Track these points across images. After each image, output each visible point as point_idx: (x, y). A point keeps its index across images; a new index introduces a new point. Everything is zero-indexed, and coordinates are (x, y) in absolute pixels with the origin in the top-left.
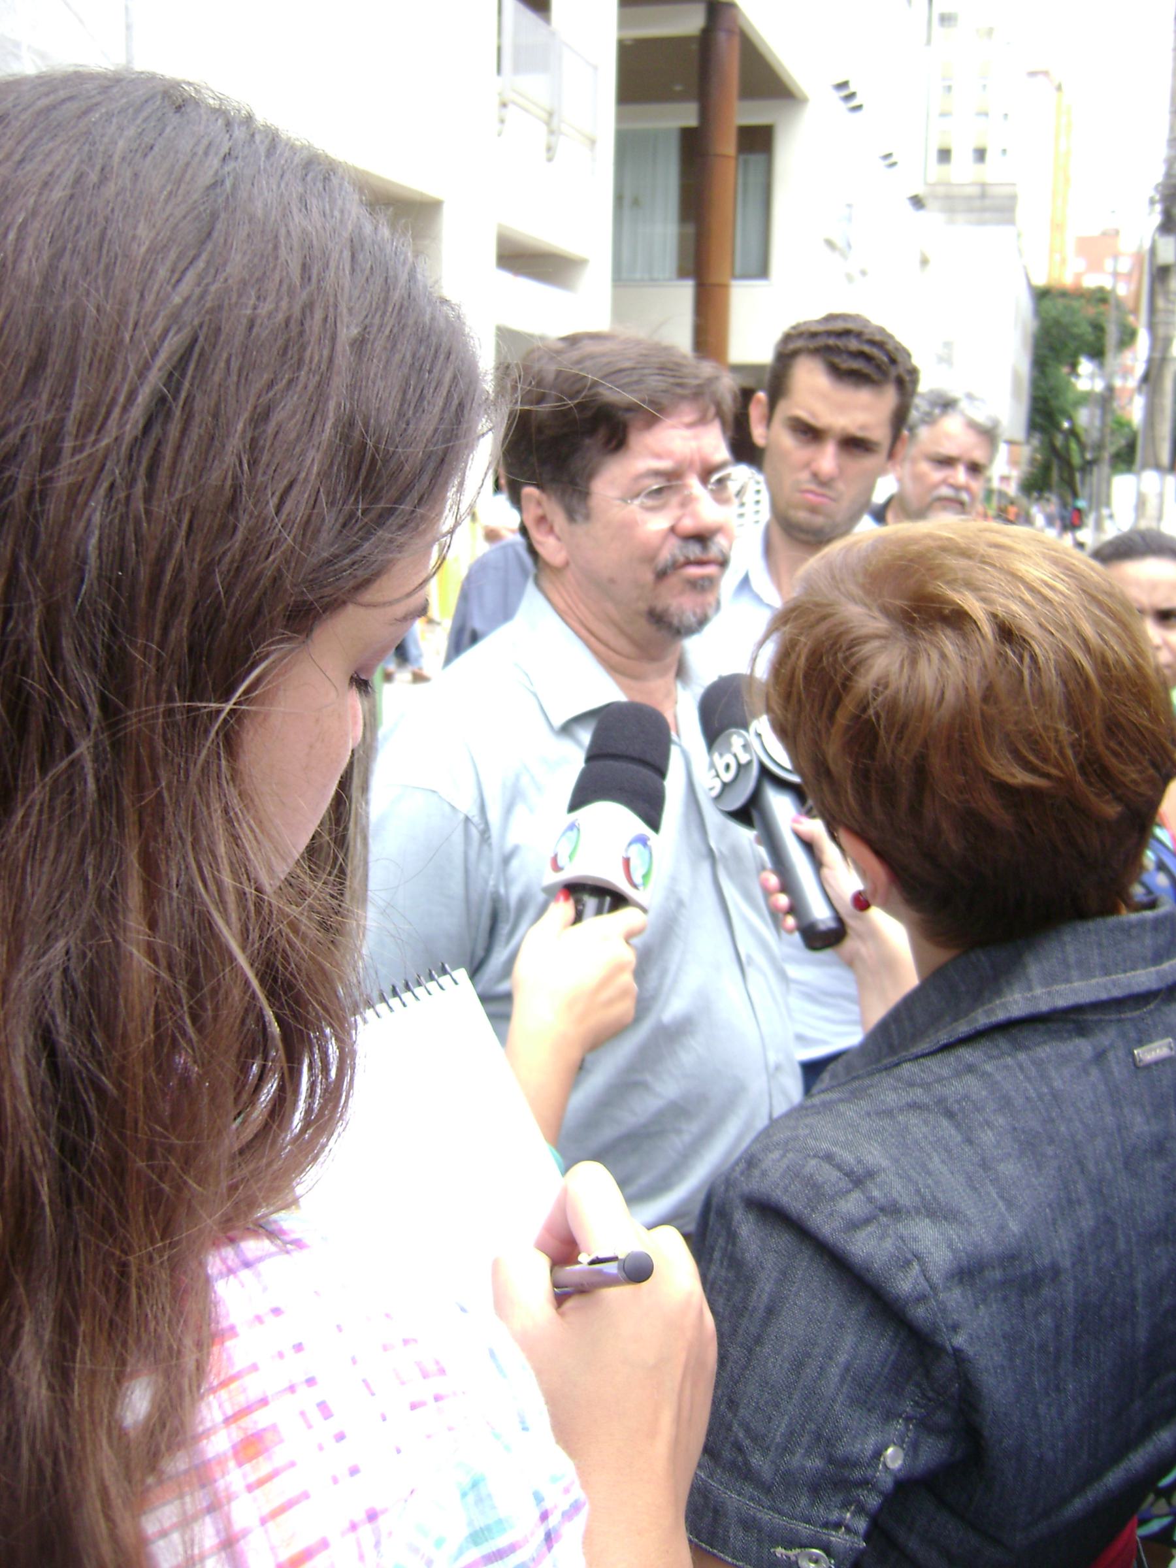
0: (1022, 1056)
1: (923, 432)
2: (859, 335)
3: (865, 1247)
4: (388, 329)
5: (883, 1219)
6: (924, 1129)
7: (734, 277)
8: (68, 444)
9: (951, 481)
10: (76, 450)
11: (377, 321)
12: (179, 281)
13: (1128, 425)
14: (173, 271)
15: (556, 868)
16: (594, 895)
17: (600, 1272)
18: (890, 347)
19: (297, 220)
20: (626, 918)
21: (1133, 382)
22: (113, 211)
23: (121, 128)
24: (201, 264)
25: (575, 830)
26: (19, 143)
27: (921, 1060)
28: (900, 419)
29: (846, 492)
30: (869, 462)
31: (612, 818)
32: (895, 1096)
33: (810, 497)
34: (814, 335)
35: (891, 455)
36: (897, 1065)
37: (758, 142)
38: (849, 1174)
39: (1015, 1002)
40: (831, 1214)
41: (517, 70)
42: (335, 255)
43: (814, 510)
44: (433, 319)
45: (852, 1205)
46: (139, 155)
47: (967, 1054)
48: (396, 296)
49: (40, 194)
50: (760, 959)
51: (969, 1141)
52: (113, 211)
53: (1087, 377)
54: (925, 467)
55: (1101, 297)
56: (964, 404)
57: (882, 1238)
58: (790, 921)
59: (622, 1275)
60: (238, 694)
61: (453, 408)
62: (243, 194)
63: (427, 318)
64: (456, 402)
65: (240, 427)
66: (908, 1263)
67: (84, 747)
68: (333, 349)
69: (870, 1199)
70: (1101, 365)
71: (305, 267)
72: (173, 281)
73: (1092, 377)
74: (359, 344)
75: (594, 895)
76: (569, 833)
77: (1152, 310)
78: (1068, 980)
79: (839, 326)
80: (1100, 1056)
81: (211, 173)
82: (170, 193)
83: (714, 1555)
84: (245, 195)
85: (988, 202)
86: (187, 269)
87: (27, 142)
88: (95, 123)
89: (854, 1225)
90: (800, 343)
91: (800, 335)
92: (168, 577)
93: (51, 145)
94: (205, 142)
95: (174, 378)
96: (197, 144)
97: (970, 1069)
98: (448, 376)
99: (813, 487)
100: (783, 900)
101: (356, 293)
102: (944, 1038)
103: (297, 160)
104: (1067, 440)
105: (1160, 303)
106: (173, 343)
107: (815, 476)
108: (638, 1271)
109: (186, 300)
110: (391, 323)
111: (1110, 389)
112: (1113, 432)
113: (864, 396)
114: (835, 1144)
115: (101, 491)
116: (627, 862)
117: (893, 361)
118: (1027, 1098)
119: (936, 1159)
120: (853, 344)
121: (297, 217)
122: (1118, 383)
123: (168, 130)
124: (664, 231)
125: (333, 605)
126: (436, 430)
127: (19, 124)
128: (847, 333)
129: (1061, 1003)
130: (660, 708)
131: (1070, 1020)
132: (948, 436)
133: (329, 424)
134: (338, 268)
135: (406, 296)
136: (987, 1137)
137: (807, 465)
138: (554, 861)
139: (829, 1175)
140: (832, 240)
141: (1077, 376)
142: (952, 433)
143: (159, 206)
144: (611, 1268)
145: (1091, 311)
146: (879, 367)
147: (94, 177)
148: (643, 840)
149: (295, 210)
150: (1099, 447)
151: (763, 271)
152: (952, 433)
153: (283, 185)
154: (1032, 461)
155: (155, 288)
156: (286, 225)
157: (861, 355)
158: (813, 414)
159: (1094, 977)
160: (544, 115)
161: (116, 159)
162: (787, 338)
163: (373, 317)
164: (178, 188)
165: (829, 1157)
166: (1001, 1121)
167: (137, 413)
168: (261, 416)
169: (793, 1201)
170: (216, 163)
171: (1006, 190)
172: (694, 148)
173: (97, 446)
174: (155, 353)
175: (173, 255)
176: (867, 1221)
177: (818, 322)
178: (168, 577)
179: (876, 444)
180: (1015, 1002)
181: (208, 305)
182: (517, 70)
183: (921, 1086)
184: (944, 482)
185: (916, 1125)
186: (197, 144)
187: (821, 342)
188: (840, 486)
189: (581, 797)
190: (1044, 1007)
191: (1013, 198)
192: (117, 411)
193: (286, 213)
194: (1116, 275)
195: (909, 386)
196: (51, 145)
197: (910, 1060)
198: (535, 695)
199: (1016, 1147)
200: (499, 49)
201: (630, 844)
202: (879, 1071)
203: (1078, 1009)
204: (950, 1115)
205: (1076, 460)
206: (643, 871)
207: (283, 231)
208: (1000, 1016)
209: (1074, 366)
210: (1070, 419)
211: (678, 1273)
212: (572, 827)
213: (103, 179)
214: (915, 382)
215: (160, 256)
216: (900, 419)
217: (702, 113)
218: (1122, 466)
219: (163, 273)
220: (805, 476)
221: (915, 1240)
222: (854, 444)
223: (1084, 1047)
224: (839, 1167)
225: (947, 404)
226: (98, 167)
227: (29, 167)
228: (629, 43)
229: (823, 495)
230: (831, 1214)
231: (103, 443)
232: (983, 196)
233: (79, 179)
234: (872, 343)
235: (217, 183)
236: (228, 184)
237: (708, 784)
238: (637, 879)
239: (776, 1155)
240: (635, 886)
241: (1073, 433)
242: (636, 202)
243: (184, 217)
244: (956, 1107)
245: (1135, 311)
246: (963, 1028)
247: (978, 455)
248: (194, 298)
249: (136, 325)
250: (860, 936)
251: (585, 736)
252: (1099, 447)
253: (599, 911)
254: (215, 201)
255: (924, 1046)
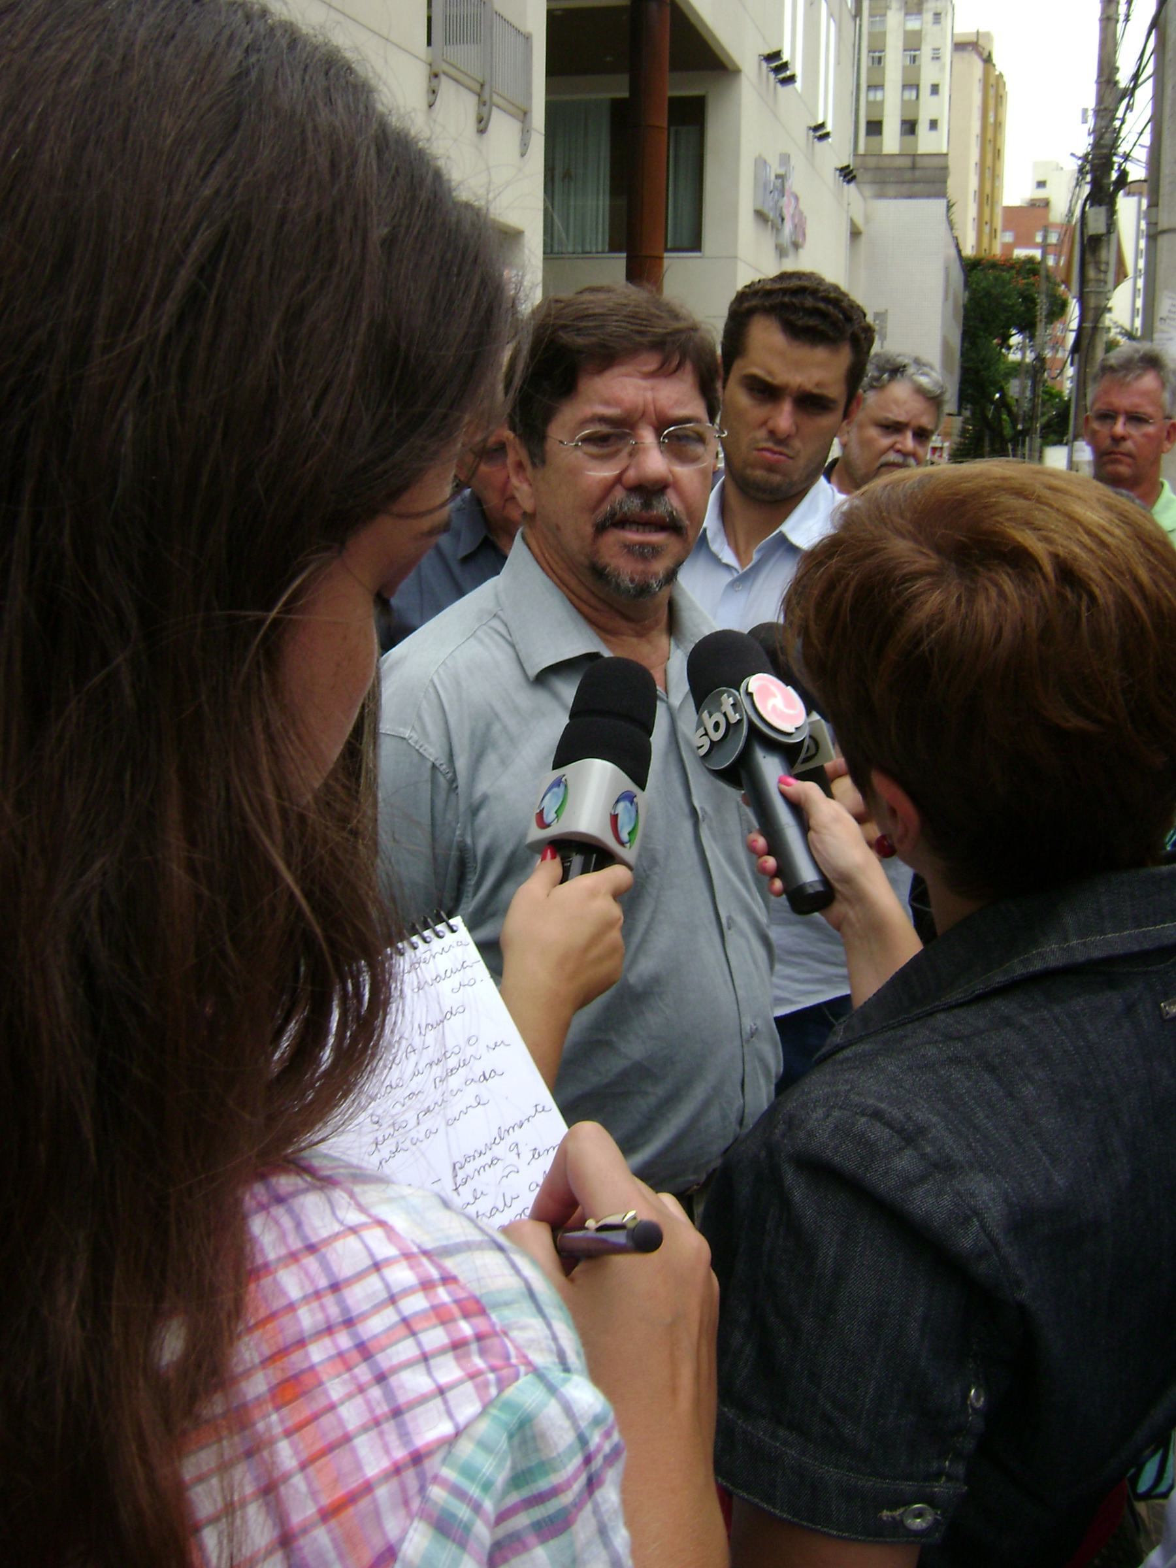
0: (1057, 1010)
1: (871, 398)
2: (814, 292)
3: (928, 1203)
4: (416, 231)
5: (938, 1176)
6: (967, 1084)
7: (667, 250)
8: (99, 341)
9: (899, 446)
10: (107, 349)
11: (404, 221)
12: (207, 174)
13: (1059, 395)
14: (200, 164)
15: (543, 824)
16: (581, 853)
17: (604, 1241)
18: (845, 304)
19: (323, 114)
20: (616, 874)
21: (1063, 354)
22: (136, 100)
23: (141, 16)
24: (230, 155)
25: (562, 787)
26: (33, 31)
27: (956, 1011)
28: (854, 376)
29: (803, 449)
30: (827, 421)
31: (598, 776)
32: (935, 1050)
33: (768, 455)
34: (769, 293)
35: (846, 415)
36: (931, 1014)
37: (691, 115)
38: (900, 1131)
39: (1051, 953)
40: (887, 1173)
41: (447, 41)
42: (363, 153)
43: (771, 468)
44: (458, 222)
45: (905, 1162)
46: (160, 44)
47: (1003, 1006)
48: (423, 195)
49: (59, 82)
50: (742, 922)
51: (1010, 1095)
52: (136, 100)
53: (1017, 350)
54: (873, 432)
55: (1030, 268)
56: (911, 370)
57: (939, 1194)
58: (778, 884)
59: (630, 1244)
60: (280, 604)
61: (482, 313)
62: (268, 87)
63: (454, 219)
64: (484, 306)
65: (274, 326)
66: (967, 1219)
67: (120, 659)
68: (364, 247)
69: (923, 1156)
70: (1032, 337)
71: (333, 165)
72: (201, 174)
73: (1022, 349)
74: (389, 243)
75: (581, 853)
76: (555, 790)
77: (1083, 281)
78: (1103, 932)
79: (794, 283)
80: (1130, 1009)
81: (235, 65)
82: (195, 82)
83: (817, 1531)
84: (270, 87)
85: (918, 174)
86: (214, 162)
87: (43, 30)
88: (112, 11)
89: (910, 1183)
90: (754, 302)
91: (755, 293)
92: (204, 480)
93: (68, 33)
94: (227, 33)
95: (205, 271)
96: (219, 34)
97: (1007, 1021)
98: (477, 281)
99: (770, 445)
100: (771, 862)
101: (384, 192)
102: (979, 988)
103: (318, 55)
104: (998, 410)
105: (1091, 273)
106: (205, 235)
107: (772, 433)
108: (647, 1239)
109: (217, 192)
110: (419, 223)
111: (1040, 359)
112: (1044, 403)
113: (820, 354)
114: (880, 1099)
115: (133, 392)
116: (614, 818)
117: (848, 319)
118: (1065, 1051)
119: (981, 1115)
120: (809, 302)
121: (324, 112)
122: (1048, 354)
123: (189, 18)
124: (596, 204)
125: (371, 512)
126: (466, 335)
127: (31, 11)
128: (802, 290)
129: (1096, 954)
130: (645, 663)
131: (1100, 973)
132: (896, 402)
133: (363, 326)
134: (365, 165)
135: (432, 197)
136: (1028, 1090)
137: (764, 423)
138: (540, 815)
139: (878, 1132)
140: (780, 196)
141: (1009, 348)
142: (899, 399)
143: (183, 96)
144: (620, 1238)
145: (1022, 282)
146: (834, 324)
147: (115, 66)
148: (629, 797)
149: (321, 104)
150: (1031, 417)
151: (695, 244)
152: (899, 399)
153: (307, 79)
154: (964, 431)
155: (184, 181)
156: (313, 120)
157: (815, 312)
158: (770, 373)
159: (1127, 929)
160: (477, 88)
161: (137, 48)
162: (742, 297)
163: (401, 217)
164: (202, 79)
165: (877, 1115)
166: (1040, 1074)
167: (171, 307)
168: (295, 316)
169: (844, 1157)
170: (240, 54)
171: (935, 162)
172: (626, 122)
173: (129, 345)
174: (187, 245)
175: (200, 147)
176: (923, 1179)
177: (774, 280)
178: (204, 480)
179: (833, 401)
180: (1051, 953)
181: (238, 200)
182: (447, 41)
183: (959, 1038)
184: (892, 447)
185: (958, 1079)
186: (219, 34)
187: (776, 300)
188: (797, 444)
189: (569, 751)
190: (1080, 957)
191: (945, 169)
192: (148, 309)
193: (312, 108)
194: (1045, 247)
195: (865, 344)
196: (68, 33)
197: (943, 1010)
198: (513, 646)
199: (1056, 1100)
200: (429, 19)
201: (617, 802)
202: (912, 1021)
203: (1109, 960)
204: (991, 1069)
205: (1008, 431)
206: (630, 829)
207: (309, 126)
208: (1038, 966)
209: (1006, 338)
210: (1001, 390)
211: (687, 1241)
212: (558, 783)
213: (125, 69)
214: (871, 342)
215: (188, 147)
216: (854, 376)
217: (636, 83)
218: (1052, 437)
219: (191, 164)
220: (762, 434)
221: (973, 1195)
222: (810, 403)
223: (1115, 1000)
224: (888, 1125)
225: (896, 370)
226: (119, 56)
227: (49, 53)
228: (559, 13)
229: (781, 454)
230: (887, 1173)
231: (138, 339)
232: (914, 168)
233: (100, 67)
234: (826, 300)
235: (242, 74)
236: (254, 75)
237: (695, 738)
238: (624, 836)
239: (820, 1113)
240: (622, 844)
241: (1004, 403)
242: (567, 176)
243: (210, 108)
244: (997, 1061)
245: (1067, 282)
246: (998, 978)
247: (926, 421)
248: (223, 192)
249: (164, 220)
250: (847, 900)
251: (568, 691)
252: (1031, 417)
253: (585, 870)
254: (241, 92)
255: (957, 995)
